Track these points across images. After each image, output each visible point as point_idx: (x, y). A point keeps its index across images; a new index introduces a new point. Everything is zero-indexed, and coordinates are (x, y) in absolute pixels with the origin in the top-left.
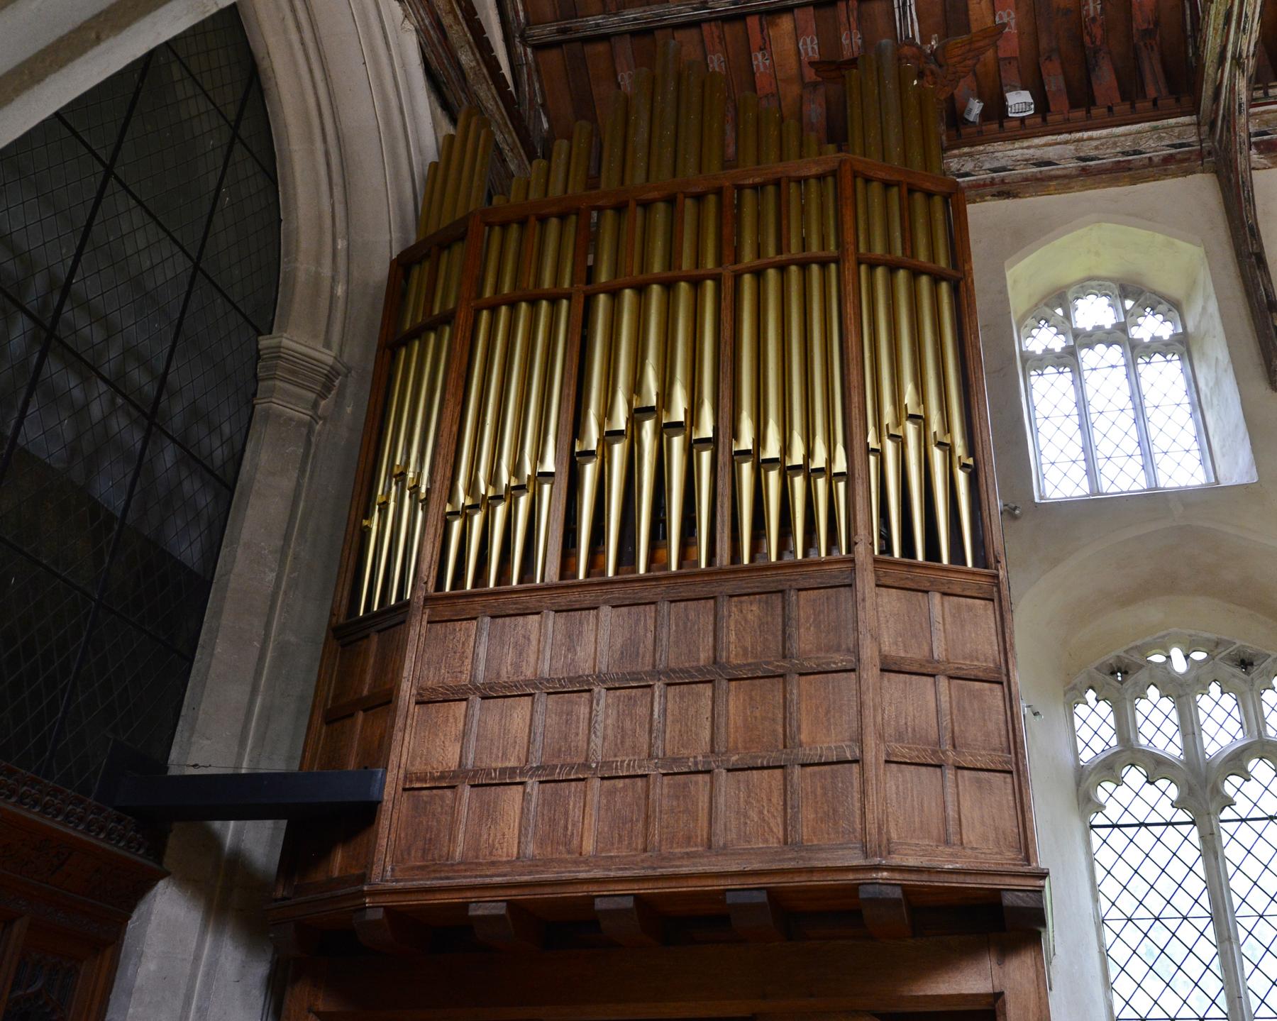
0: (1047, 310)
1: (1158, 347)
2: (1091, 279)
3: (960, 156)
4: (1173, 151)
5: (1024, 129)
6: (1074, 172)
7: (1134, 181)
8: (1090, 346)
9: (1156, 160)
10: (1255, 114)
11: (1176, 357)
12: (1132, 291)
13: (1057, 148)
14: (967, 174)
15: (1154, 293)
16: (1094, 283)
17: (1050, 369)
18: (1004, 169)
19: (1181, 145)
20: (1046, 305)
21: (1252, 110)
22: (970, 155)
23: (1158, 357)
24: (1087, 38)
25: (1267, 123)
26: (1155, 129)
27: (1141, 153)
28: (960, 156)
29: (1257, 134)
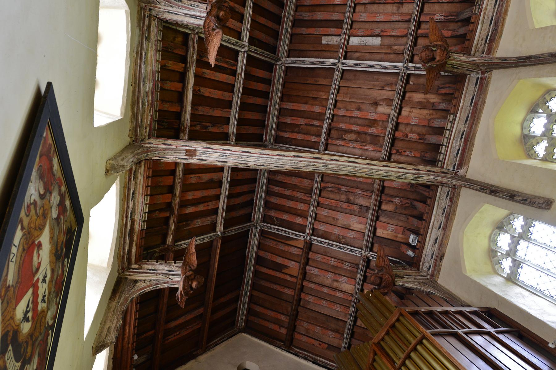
0: (496, 258)
1: (527, 227)
2: (490, 237)
3: (423, 266)
4: (449, 197)
5: (422, 243)
6: (443, 232)
7: (455, 214)
8: (516, 251)
9: (450, 204)
10: (447, 167)
11: (534, 222)
12: (501, 226)
13: (433, 234)
14: (430, 267)
15: (504, 218)
16: (492, 236)
17: (519, 270)
18: (433, 255)
19: (448, 194)
20: (493, 257)
21: (445, 167)
22: (424, 262)
23: (531, 229)
24: (407, 205)
25: (451, 163)
26: (439, 201)
27: (445, 208)
28: (423, 266)
29: (454, 168)
